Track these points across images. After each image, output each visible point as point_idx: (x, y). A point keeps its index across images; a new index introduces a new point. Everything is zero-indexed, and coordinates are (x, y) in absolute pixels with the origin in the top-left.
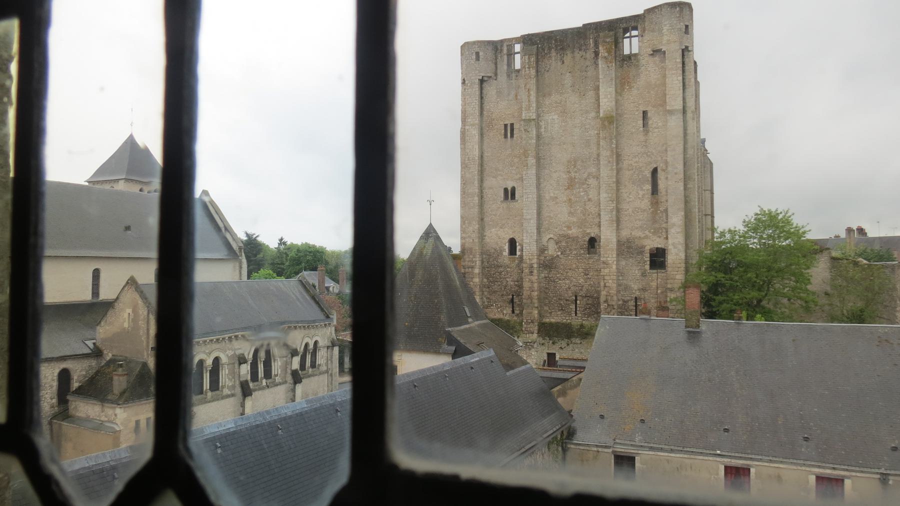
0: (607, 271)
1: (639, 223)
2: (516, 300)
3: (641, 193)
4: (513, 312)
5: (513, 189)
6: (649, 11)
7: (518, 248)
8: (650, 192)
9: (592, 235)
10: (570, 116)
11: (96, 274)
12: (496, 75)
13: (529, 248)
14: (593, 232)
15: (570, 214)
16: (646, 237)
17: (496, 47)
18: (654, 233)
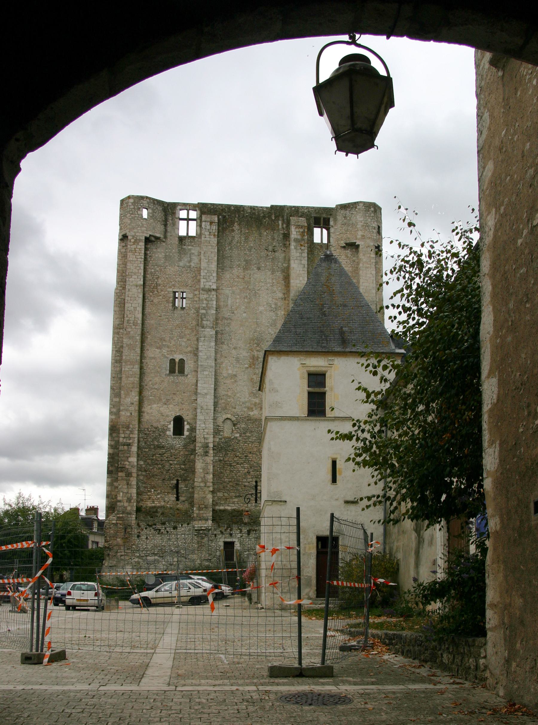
2: (182, 486)
4: (177, 499)
5: (182, 361)
6: (344, 207)
7: (186, 427)
11: (317, 379)
12: (165, 237)
13: (204, 429)
17: (168, 211)
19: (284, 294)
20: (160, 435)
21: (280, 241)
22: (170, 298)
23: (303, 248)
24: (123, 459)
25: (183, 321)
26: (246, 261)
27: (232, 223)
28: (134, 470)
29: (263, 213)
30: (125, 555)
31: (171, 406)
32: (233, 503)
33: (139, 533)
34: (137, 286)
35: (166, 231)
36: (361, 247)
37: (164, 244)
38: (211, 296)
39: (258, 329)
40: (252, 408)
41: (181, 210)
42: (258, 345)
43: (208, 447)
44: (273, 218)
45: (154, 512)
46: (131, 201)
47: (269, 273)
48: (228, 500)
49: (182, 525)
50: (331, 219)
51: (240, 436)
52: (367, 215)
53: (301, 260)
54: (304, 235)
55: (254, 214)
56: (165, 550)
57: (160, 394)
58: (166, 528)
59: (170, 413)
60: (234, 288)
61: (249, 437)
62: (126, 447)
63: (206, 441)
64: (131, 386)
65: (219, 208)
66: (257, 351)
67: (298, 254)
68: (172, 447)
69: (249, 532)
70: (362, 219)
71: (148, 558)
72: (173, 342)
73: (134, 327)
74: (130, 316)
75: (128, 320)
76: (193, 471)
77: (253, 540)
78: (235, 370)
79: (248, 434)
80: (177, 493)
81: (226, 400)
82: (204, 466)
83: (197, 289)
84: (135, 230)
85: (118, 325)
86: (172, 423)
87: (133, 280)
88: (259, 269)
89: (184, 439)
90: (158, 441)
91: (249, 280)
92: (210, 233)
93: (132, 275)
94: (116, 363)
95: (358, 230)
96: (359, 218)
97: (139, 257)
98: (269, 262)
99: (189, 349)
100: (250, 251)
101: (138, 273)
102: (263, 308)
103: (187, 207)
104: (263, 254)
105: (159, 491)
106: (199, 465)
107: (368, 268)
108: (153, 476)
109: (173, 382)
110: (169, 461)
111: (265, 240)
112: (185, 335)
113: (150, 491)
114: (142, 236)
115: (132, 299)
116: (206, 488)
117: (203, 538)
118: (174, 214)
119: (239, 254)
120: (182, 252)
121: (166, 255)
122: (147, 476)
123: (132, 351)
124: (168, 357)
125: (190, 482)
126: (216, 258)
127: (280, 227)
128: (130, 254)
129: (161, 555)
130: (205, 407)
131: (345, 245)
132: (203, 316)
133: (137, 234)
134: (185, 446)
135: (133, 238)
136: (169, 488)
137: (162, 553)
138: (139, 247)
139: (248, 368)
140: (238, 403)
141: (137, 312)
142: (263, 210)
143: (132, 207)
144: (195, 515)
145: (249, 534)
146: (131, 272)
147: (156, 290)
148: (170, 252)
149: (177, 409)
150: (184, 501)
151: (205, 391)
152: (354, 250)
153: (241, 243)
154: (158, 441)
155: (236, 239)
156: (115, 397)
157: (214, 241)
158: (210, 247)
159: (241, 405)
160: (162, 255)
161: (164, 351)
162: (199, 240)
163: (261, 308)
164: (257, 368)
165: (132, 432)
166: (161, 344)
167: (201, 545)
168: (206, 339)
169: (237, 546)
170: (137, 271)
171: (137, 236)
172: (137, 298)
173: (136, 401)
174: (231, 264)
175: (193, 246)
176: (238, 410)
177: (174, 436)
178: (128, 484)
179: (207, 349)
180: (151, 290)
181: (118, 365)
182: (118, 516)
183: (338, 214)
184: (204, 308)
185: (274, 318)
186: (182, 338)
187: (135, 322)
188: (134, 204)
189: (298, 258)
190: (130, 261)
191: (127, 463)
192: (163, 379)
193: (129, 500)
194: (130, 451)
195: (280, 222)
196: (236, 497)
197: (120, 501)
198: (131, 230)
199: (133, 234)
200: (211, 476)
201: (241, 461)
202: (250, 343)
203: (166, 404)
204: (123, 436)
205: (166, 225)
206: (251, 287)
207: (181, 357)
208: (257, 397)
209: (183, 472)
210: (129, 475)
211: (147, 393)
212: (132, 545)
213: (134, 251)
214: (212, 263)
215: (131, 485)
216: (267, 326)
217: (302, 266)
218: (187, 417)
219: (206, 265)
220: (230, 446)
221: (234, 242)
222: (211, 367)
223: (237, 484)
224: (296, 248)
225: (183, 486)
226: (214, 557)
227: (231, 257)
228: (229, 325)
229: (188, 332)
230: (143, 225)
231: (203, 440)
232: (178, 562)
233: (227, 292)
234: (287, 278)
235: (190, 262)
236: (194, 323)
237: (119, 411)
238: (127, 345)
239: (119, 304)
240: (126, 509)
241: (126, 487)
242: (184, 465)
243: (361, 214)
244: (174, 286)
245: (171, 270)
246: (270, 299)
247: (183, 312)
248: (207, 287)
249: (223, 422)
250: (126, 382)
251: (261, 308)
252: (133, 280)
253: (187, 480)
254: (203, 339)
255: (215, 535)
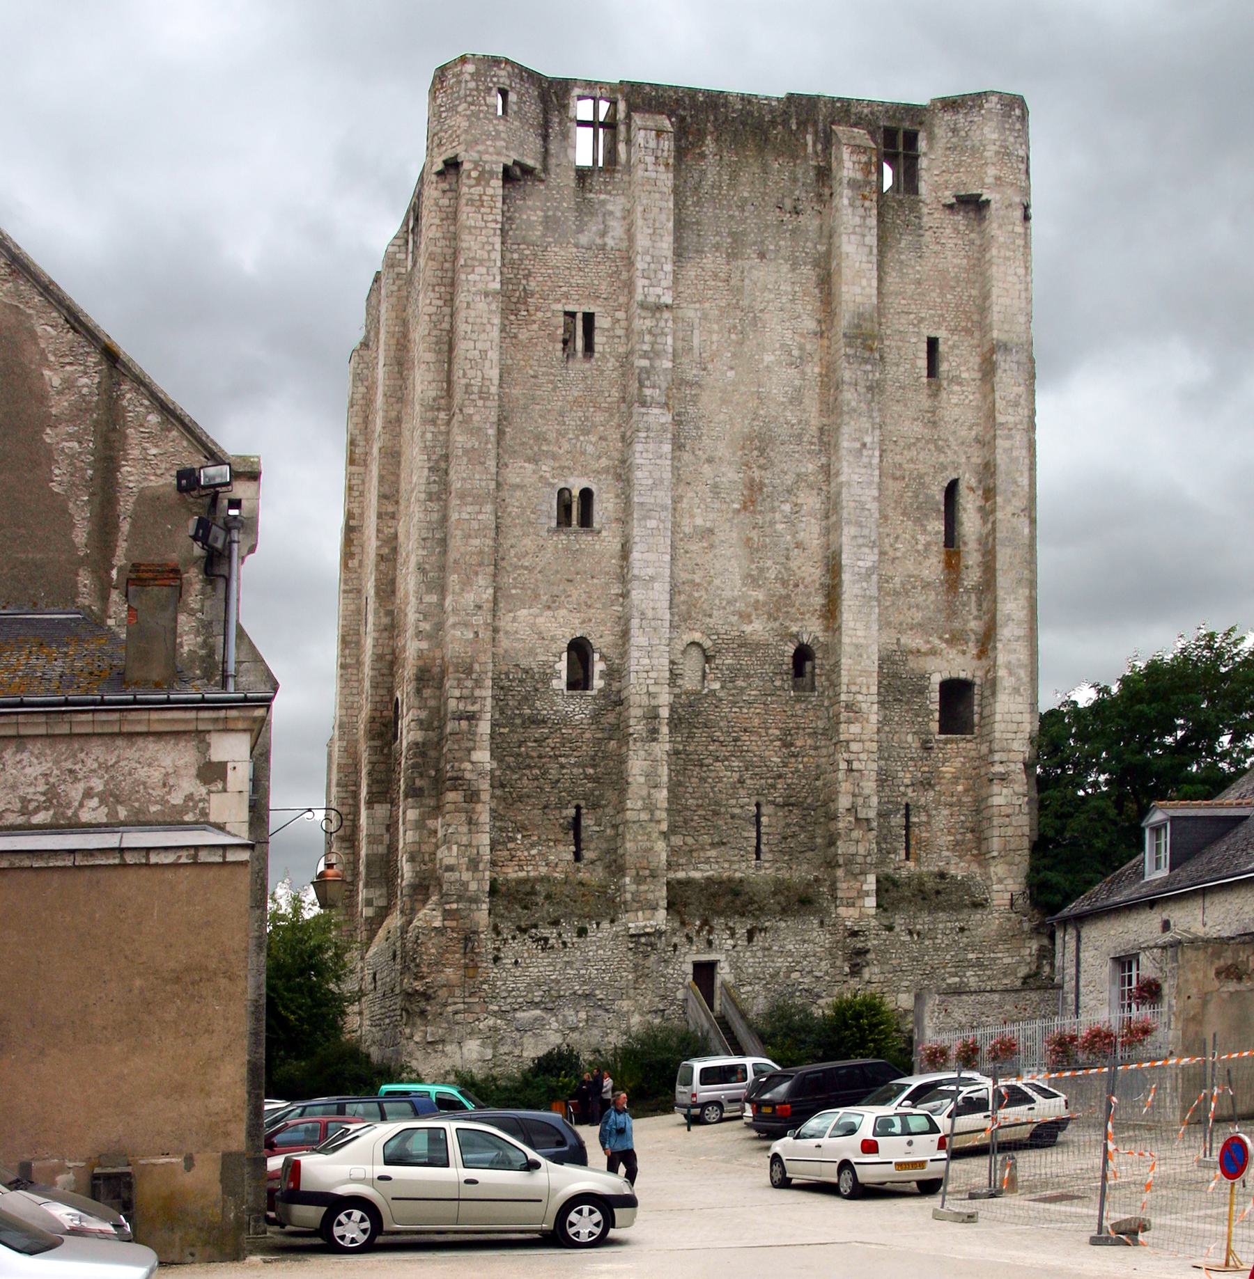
0: (855, 729)
1: (918, 616)
2: (587, 821)
3: (922, 539)
4: (578, 856)
5: (586, 495)
7: (599, 667)
8: (942, 538)
9: (805, 639)
10: (741, 324)
12: (545, 169)
14: (811, 630)
15: (753, 580)
16: (933, 652)
18: (950, 642)
19: (819, 322)
20: (537, 690)
21: (810, 185)
22: (557, 328)
23: (867, 204)
24: (458, 755)
25: (589, 389)
26: (731, 234)
27: (701, 135)
28: (485, 785)
29: (771, 112)
30: (465, 1011)
31: (563, 612)
32: (707, 861)
33: (498, 949)
34: (486, 295)
35: (546, 153)
36: (993, 206)
37: (542, 187)
38: (662, 324)
39: (762, 412)
40: (749, 616)
41: (580, 98)
42: (762, 451)
43: (656, 717)
44: (794, 127)
45: (528, 894)
46: (470, 68)
47: (785, 268)
48: (695, 854)
49: (598, 924)
50: (922, 136)
51: (722, 687)
52: (1007, 126)
53: (864, 236)
54: (870, 172)
55: (750, 113)
56: (558, 991)
57: (537, 580)
58: (560, 935)
59: (559, 632)
60: (707, 305)
61: (742, 689)
62: (464, 723)
63: (654, 703)
64: (474, 560)
65: (670, 97)
66: (760, 467)
67: (858, 220)
68: (565, 720)
69: (751, 935)
70: (995, 136)
71: (519, 1015)
72: (566, 446)
73: (480, 403)
74: (470, 373)
75: (468, 386)
76: (620, 783)
77: (759, 954)
78: (711, 516)
79: (740, 683)
80: (578, 841)
81: (690, 595)
82: (646, 766)
83: (620, 305)
84: (480, 148)
85: (434, 400)
86: (565, 656)
87: (478, 278)
88: (762, 256)
89: (594, 698)
90: (532, 707)
91: (739, 284)
92: (657, 158)
93: (474, 267)
94: (430, 500)
95: (986, 164)
96: (988, 133)
97: (491, 217)
98: (784, 239)
99: (604, 462)
100: (742, 208)
101: (489, 259)
102: (772, 358)
103: (592, 89)
104: (772, 217)
105: (535, 838)
106: (636, 766)
107: (1008, 259)
108: (520, 799)
109: (566, 549)
110: (557, 757)
111: (777, 183)
112: (594, 426)
113: (514, 840)
114: (497, 163)
115: (476, 328)
116: (653, 824)
117: (646, 957)
118: (564, 107)
119: (716, 217)
120: (584, 208)
121: (546, 217)
122: (505, 799)
123: (478, 468)
124: (553, 485)
125: (607, 810)
126: (671, 225)
127: (810, 149)
128: (469, 209)
129: (550, 1005)
130: (650, 614)
131: (954, 200)
132: (644, 376)
133: (486, 157)
134: (596, 717)
135: (475, 169)
136: (557, 829)
137: (551, 1003)
138: (490, 191)
139: (739, 511)
140: (717, 602)
141: (487, 364)
142: (769, 105)
143: (472, 85)
144: (628, 896)
145: (750, 940)
146: (473, 259)
147: (523, 307)
148: (557, 209)
149: (577, 621)
150: (592, 862)
151: (650, 571)
152: (972, 215)
153: (720, 187)
154: (532, 707)
155: (711, 177)
156: (427, 593)
157: (666, 179)
158: (657, 196)
159: (724, 608)
160: (536, 217)
161: (544, 468)
162: (626, 178)
163: (768, 358)
164: (761, 512)
165: (478, 684)
166: (536, 448)
167: (641, 974)
168: (652, 435)
169: (724, 974)
170: (486, 256)
171: (486, 162)
172: (488, 327)
173: (487, 601)
174: (698, 242)
175: (609, 193)
176: (716, 620)
177: (570, 692)
178: (470, 822)
179: (651, 461)
180: (513, 307)
181: (434, 506)
182: (447, 907)
183: (937, 121)
184: (645, 355)
185: (797, 383)
186: (588, 434)
187: (485, 389)
188: (475, 76)
189: (857, 229)
190: (470, 228)
191: (468, 766)
192: (542, 542)
193: (474, 864)
194: (475, 734)
195: (809, 138)
196: (713, 845)
197: (450, 868)
198: (470, 145)
199: (475, 156)
200: (665, 793)
201: (724, 752)
202: (743, 448)
203: (549, 607)
204: (457, 693)
205: (545, 138)
206: (744, 303)
207: (585, 483)
208: (760, 586)
209: (589, 785)
210: (472, 797)
211: (505, 580)
212: (482, 983)
213: (478, 203)
214: (662, 236)
215: (477, 824)
216: (783, 403)
217: (867, 250)
218: (602, 640)
219: (648, 243)
220: (700, 713)
221: (706, 186)
222: (664, 508)
223: (715, 813)
224: (852, 205)
225: (591, 822)
226: (671, 1005)
227: (697, 223)
228: (695, 400)
229: (600, 417)
230: (498, 132)
231: (645, 700)
232: (587, 1021)
233: (691, 314)
234: (826, 282)
235: (603, 234)
236: (616, 394)
237: (439, 626)
238: (466, 452)
239: (437, 343)
240: (467, 890)
241: (465, 829)
242: (594, 766)
243: (993, 124)
244: (566, 296)
245: (559, 255)
246: (789, 334)
247: (588, 366)
248: (651, 299)
249: (684, 652)
250: (462, 549)
251: (768, 358)
252: (478, 278)
253: (599, 807)
254: (644, 435)
255: (675, 946)
